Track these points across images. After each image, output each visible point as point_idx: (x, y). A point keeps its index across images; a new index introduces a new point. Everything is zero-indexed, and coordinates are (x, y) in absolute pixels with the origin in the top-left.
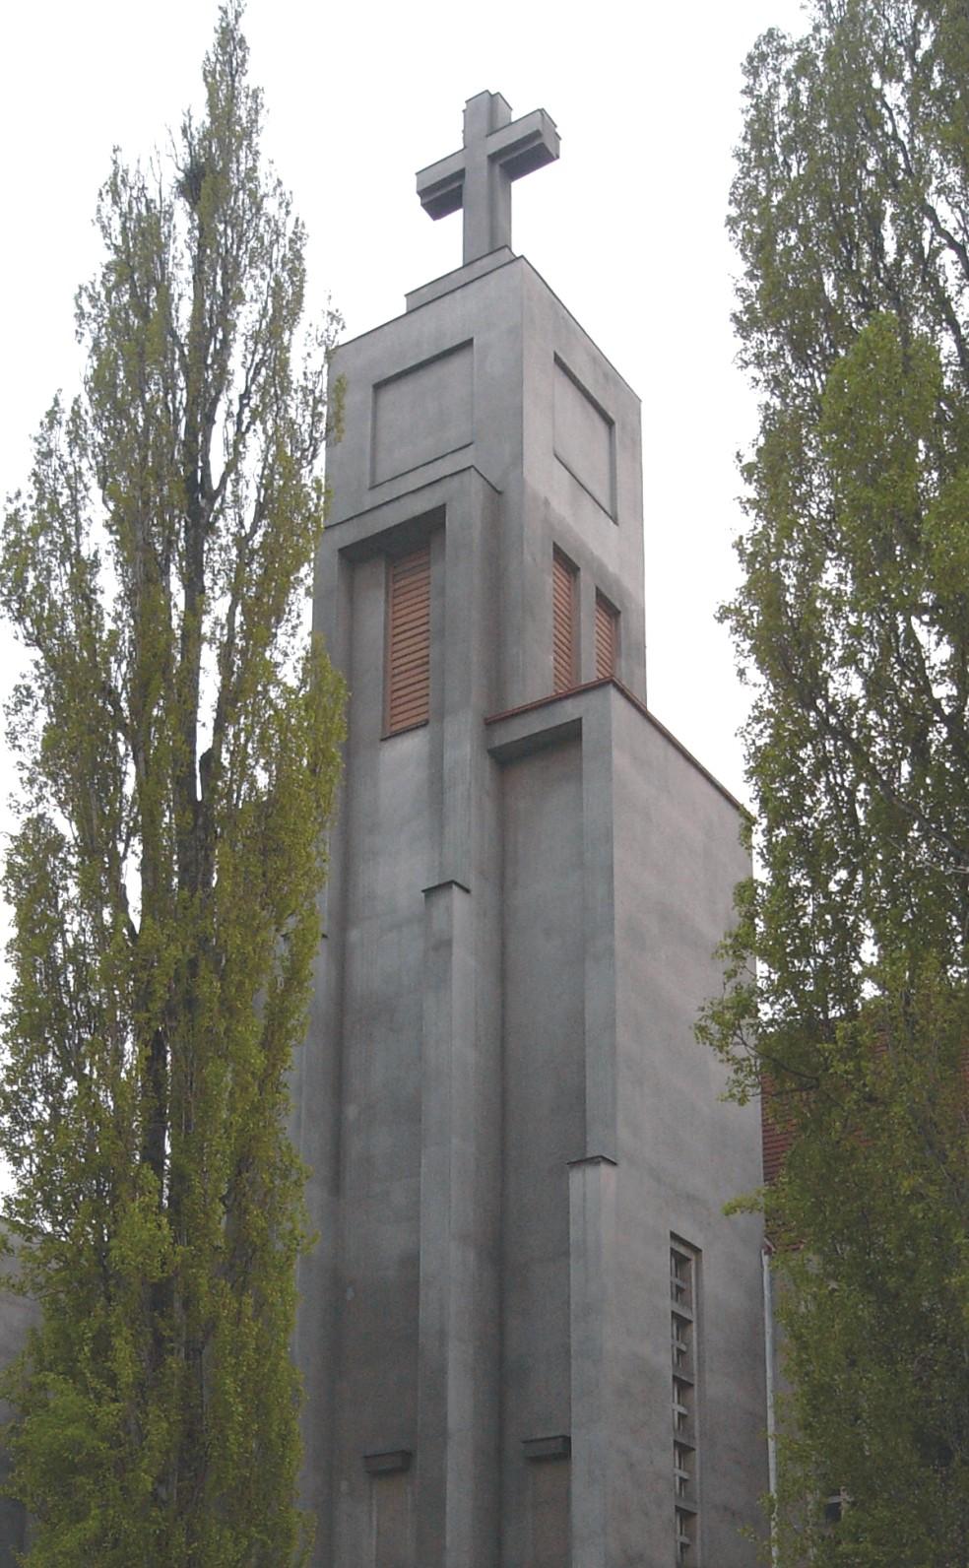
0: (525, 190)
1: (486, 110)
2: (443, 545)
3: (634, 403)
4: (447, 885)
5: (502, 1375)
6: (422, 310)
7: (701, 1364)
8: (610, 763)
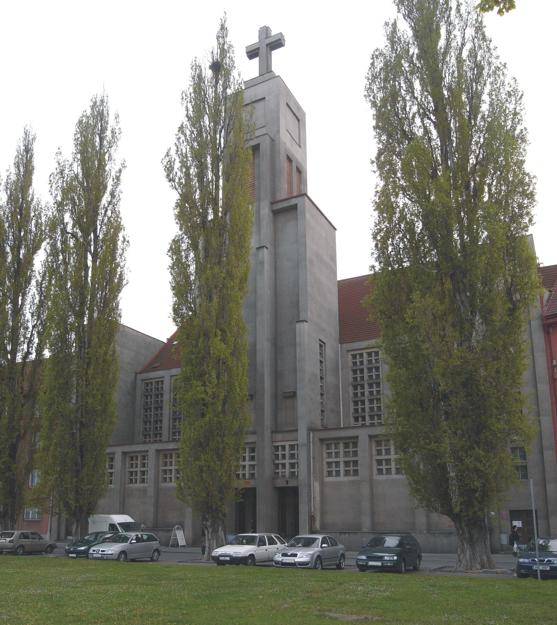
0: (275, 54)
1: (265, 31)
3: (304, 114)
5: (277, 376)
7: (326, 373)
8: (305, 217)
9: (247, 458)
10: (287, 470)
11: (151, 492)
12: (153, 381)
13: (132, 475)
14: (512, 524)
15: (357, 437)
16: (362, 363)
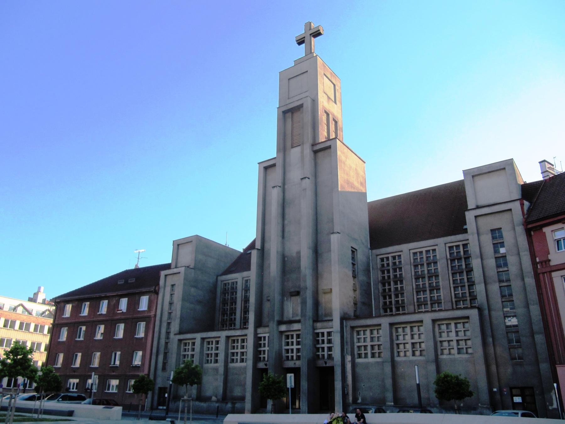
2: (340, 314)
4: (305, 178)
6: (505, 212)
9: (295, 343)
10: (326, 353)
11: (221, 370)
12: (390, 256)
13: (208, 357)
14: (513, 400)
15: (421, 321)
16: (388, 265)
